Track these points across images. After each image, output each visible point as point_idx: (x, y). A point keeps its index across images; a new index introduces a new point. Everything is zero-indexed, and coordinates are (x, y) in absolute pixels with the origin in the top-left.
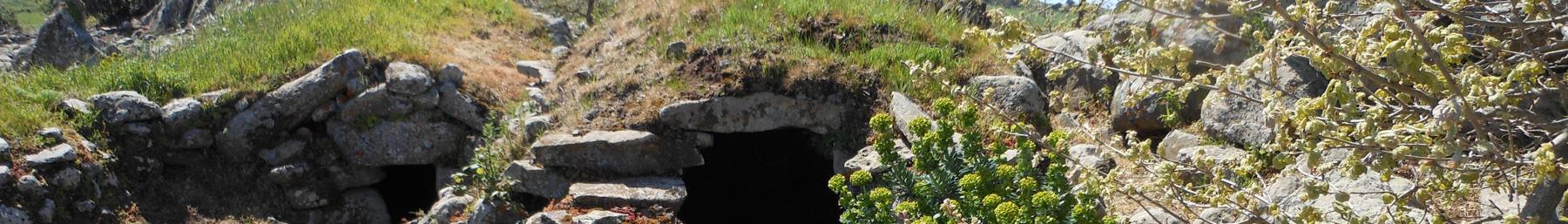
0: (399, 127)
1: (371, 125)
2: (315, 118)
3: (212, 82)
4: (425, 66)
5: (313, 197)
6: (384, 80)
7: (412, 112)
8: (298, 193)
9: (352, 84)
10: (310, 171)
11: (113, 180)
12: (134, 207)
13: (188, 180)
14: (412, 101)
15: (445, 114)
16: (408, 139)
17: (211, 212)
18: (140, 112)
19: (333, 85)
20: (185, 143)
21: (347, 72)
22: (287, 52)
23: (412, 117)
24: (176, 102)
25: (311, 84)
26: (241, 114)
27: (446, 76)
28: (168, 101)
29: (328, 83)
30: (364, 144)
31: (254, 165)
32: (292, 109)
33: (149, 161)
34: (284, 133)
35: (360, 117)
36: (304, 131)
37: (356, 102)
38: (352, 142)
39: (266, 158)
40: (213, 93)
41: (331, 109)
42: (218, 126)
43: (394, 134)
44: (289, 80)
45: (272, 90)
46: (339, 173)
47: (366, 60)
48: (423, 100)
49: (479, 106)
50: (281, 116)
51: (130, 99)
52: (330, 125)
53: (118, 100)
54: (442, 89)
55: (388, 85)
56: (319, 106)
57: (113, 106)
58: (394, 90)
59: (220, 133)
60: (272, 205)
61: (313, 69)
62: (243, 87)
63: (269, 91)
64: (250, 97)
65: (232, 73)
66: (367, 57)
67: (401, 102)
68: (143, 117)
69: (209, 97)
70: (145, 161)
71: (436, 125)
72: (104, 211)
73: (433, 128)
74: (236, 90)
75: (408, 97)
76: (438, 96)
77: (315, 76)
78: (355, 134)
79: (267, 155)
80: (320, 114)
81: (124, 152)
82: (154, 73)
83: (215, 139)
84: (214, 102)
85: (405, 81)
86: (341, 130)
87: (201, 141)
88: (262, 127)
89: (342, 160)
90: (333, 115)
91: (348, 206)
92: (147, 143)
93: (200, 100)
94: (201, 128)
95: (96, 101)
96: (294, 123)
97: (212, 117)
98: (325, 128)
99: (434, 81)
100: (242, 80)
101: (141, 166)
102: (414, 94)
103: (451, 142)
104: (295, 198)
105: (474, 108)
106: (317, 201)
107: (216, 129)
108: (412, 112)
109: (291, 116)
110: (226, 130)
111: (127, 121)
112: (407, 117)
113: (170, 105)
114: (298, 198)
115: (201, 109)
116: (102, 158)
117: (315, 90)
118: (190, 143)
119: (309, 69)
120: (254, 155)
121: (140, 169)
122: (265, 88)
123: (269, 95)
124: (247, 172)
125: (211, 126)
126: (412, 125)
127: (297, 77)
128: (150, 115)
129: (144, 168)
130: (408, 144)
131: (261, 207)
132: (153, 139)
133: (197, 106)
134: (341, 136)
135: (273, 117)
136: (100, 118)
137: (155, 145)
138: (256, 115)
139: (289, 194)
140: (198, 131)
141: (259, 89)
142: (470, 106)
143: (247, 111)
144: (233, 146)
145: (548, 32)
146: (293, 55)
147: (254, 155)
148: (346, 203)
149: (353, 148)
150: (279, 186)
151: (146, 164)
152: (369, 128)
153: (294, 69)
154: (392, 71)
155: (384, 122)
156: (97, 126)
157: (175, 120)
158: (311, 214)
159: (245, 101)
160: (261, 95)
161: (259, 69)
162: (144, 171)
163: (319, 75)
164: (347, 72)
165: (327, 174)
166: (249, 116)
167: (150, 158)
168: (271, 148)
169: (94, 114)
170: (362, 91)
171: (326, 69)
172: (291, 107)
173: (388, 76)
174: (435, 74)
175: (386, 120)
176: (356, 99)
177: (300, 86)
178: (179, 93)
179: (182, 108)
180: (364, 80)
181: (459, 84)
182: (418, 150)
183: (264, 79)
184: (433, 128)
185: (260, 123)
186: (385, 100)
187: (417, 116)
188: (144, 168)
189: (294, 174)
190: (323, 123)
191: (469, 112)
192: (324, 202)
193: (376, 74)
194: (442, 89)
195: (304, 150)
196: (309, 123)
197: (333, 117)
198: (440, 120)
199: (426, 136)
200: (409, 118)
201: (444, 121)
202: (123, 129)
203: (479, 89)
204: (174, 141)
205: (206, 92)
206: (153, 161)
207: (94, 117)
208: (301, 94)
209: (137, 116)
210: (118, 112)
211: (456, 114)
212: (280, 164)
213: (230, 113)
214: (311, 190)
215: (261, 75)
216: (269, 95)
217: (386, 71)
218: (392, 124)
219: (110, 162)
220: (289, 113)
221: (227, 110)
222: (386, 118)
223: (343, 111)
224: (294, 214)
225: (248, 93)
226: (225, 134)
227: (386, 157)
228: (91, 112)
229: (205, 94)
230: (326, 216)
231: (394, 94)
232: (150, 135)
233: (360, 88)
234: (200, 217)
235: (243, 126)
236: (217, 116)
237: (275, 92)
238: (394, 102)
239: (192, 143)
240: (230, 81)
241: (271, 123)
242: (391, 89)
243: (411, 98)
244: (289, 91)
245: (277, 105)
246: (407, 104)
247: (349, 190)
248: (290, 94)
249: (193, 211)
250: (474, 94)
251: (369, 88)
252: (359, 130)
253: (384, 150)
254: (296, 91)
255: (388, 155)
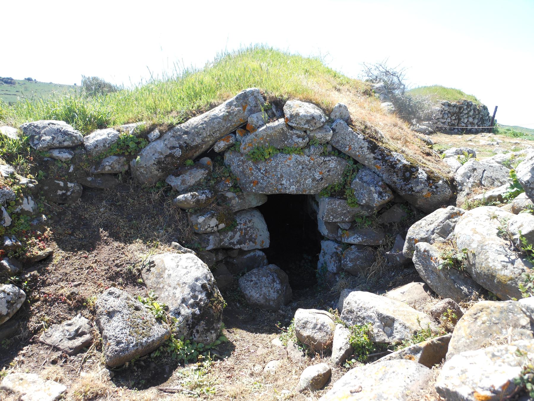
0: (293, 160)
1: (267, 157)
2: (216, 149)
3: (131, 116)
4: (318, 105)
5: (213, 222)
6: (283, 115)
7: (308, 146)
8: (201, 219)
9: (253, 119)
10: (212, 197)
11: (28, 205)
12: (48, 232)
13: (104, 203)
14: (308, 136)
15: (334, 149)
16: (302, 172)
17: (120, 235)
18: (63, 139)
19: (115, 170)
20: (104, 168)
21: (248, 108)
22: (193, 93)
23: (306, 151)
24: (99, 131)
25: (216, 117)
26: (153, 144)
27: (338, 114)
28: (92, 131)
29: (230, 117)
30: (260, 174)
31: (162, 189)
32: (198, 140)
33: (70, 185)
34: (189, 162)
35: (258, 149)
36: (206, 160)
37: (256, 135)
38: (248, 172)
39: (172, 184)
40: (131, 125)
41: (231, 141)
42: (132, 154)
43: (289, 166)
44: (194, 115)
45: (180, 123)
46: (234, 198)
47: (265, 98)
48: (319, 135)
49: (370, 142)
50: (186, 146)
51: (56, 127)
52: (228, 156)
53: (44, 127)
54: (334, 126)
55: (287, 120)
56: (220, 138)
57: (39, 133)
58: (293, 125)
59: (134, 160)
60: (176, 230)
61: (215, 106)
62: (156, 121)
63: (177, 124)
64: (161, 128)
65: (148, 108)
66: (265, 95)
67: (299, 137)
68: (66, 144)
69: (127, 128)
70: (66, 184)
71: (327, 159)
72: (8, 242)
73: (324, 161)
74: (150, 123)
75: (305, 132)
76: (332, 132)
77: (220, 111)
78: (252, 164)
79: (175, 182)
80: (221, 145)
81: (46, 177)
82: (83, 107)
83: (129, 166)
84: (130, 132)
85: (305, 116)
86: (239, 160)
87: (117, 167)
88: (171, 155)
89: (237, 187)
90: (232, 147)
91: (239, 227)
92: (69, 168)
93: (119, 131)
94: (118, 155)
95: (25, 128)
96: (197, 154)
97: (128, 146)
98: (223, 158)
99: (327, 118)
100: (156, 113)
101: (61, 190)
102: (311, 129)
103: (338, 175)
104: (197, 224)
105: (366, 144)
106: (217, 226)
107: (131, 157)
108: (308, 146)
109: (197, 146)
110: (139, 157)
111: (51, 148)
112: (301, 151)
113: (92, 135)
114: (200, 223)
115: (119, 138)
116: (18, 184)
117: (219, 123)
118: (108, 168)
119: (212, 106)
120: (163, 181)
121: (60, 192)
122: (175, 121)
123: (178, 127)
124: (155, 196)
125: (127, 154)
126: (307, 158)
127: (202, 112)
128: (73, 142)
129: (64, 192)
130: (300, 175)
131: (167, 232)
132: (74, 164)
133: (115, 135)
134: (239, 166)
135: (181, 147)
136: (27, 144)
137: (75, 169)
138: (166, 145)
139: (193, 219)
140: (115, 158)
141: (169, 122)
142: (363, 142)
143: (159, 141)
144: (145, 172)
145: (375, 92)
146: (197, 95)
147: (163, 181)
148: (238, 225)
149: (249, 178)
150: (183, 210)
151: (66, 189)
152: (266, 160)
153: (199, 106)
154: (290, 107)
155: (279, 154)
156: (22, 151)
157: (95, 147)
158: (211, 237)
159: (156, 132)
160: (171, 127)
161: (170, 105)
162: (63, 194)
163: (223, 109)
164: (248, 108)
165: (224, 199)
166: (159, 146)
167: (71, 182)
168: (177, 175)
169: (21, 140)
170: (263, 125)
171: (230, 104)
172: (196, 138)
173: (287, 112)
174: (327, 111)
175: (282, 153)
176: (257, 132)
177: (206, 119)
178: (102, 125)
179: (103, 137)
180: (264, 115)
181: (349, 122)
182: (309, 181)
183: (174, 114)
184: (324, 161)
185: (169, 152)
186: (283, 134)
187: (312, 150)
188: (64, 192)
189: (198, 200)
190: (222, 154)
191: (361, 148)
192: (222, 226)
193: (274, 110)
194: (334, 126)
195: (205, 178)
196: (210, 153)
197: (232, 148)
198: (329, 155)
199: (318, 170)
200: (304, 152)
201: (334, 155)
202: (48, 155)
203: (366, 127)
204: (94, 167)
205: (125, 124)
206: (73, 185)
207: (20, 142)
208: (207, 126)
209: (60, 143)
210: (43, 138)
211: (347, 149)
212: (185, 191)
213: (144, 143)
214: (212, 216)
215: (172, 111)
216: (178, 127)
217: (285, 107)
218: (288, 156)
219: (27, 187)
220: (195, 143)
221: (141, 139)
222: (281, 150)
223: (243, 144)
224: (196, 238)
225: (160, 125)
226: (138, 161)
227: (280, 187)
228: (18, 138)
229: (124, 126)
230: (222, 237)
231: (292, 128)
232: (72, 161)
233: (260, 123)
234: (110, 240)
235: (154, 154)
236: (132, 145)
237: (182, 125)
238: (291, 137)
239: (110, 168)
240: (145, 115)
241: (178, 153)
242: (290, 124)
243: (308, 132)
244: (196, 123)
245: (185, 136)
246: (304, 139)
247: (241, 212)
248: (196, 127)
249: (104, 234)
250: (363, 132)
251: (269, 122)
252: (256, 161)
253: (279, 180)
254: (202, 124)
255: (281, 184)
